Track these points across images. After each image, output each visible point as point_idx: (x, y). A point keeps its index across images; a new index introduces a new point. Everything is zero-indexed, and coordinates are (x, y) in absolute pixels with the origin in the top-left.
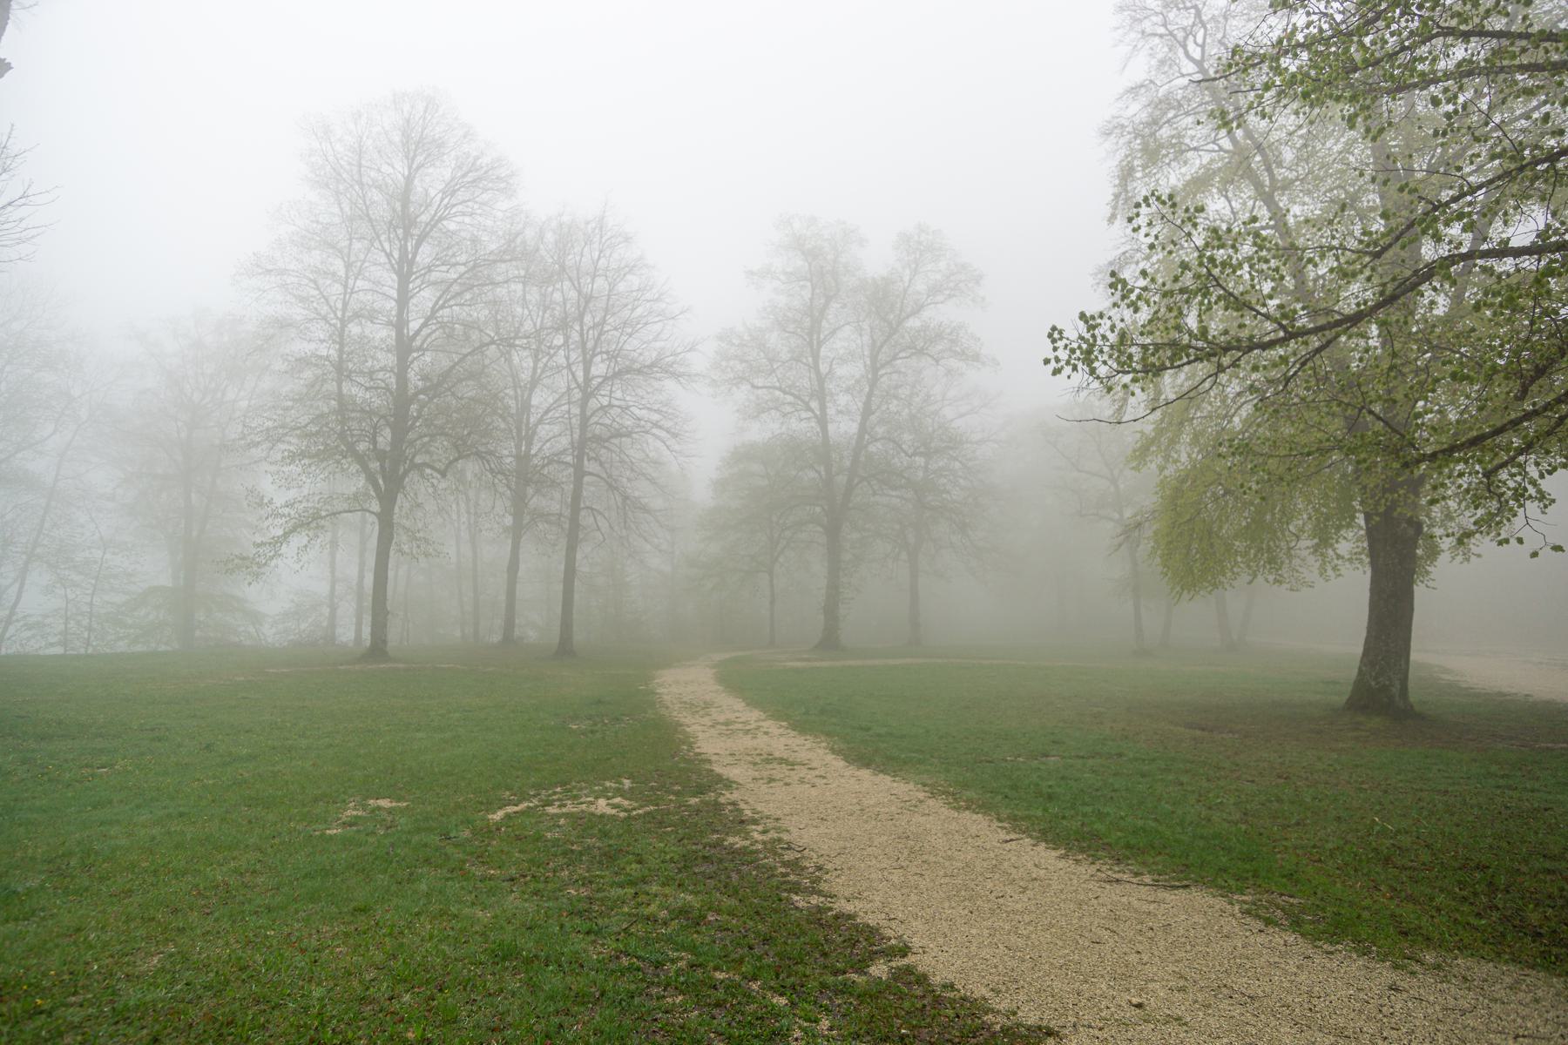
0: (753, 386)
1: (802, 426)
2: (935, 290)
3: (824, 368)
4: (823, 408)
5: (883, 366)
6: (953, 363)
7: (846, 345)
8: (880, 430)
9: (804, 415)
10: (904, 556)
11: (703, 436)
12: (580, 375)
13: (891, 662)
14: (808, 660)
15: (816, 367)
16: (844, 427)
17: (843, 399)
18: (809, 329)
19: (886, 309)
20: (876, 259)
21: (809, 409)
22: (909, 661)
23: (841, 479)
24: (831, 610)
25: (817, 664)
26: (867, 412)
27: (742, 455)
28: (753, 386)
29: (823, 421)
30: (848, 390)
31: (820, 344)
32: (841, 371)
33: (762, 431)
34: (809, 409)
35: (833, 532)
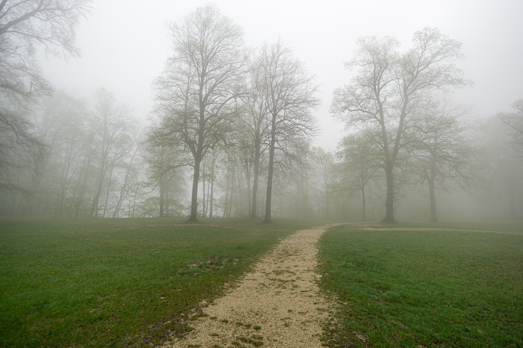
0: (350, 110)
1: (372, 125)
2: (434, 56)
3: (382, 100)
4: (382, 116)
5: (410, 94)
6: (447, 87)
7: (391, 91)
8: (411, 124)
9: (373, 120)
10: (426, 181)
11: (329, 133)
12: (201, 69)
13: (420, 229)
14: (377, 227)
15: (378, 99)
16: (393, 124)
17: (390, 111)
18: (374, 82)
19: (414, 74)
20: (405, 46)
21: (375, 117)
22: (430, 229)
23: (391, 146)
24: (390, 204)
25: (381, 229)
26: (403, 116)
27: (348, 141)
28: (350, 110)
29: (382, 122)
30: (393, 107)
31: (379, 89)
32: (389, 100)
33: (357, 129)
34: (375, 117)
35: (389, 170)
